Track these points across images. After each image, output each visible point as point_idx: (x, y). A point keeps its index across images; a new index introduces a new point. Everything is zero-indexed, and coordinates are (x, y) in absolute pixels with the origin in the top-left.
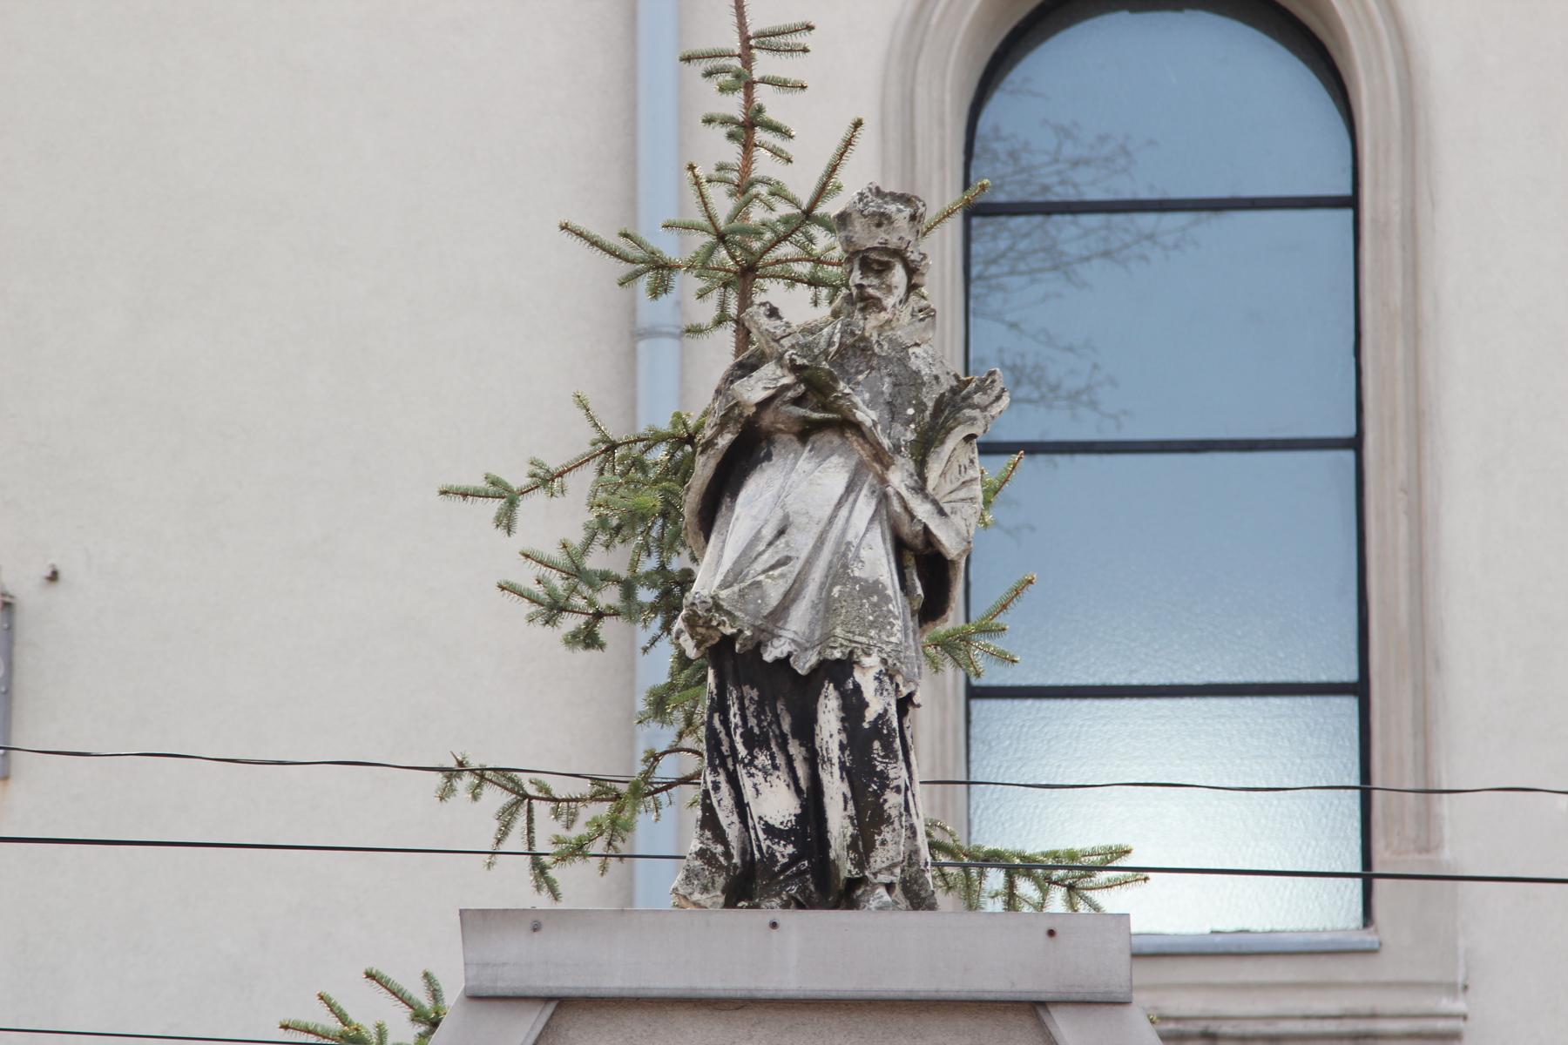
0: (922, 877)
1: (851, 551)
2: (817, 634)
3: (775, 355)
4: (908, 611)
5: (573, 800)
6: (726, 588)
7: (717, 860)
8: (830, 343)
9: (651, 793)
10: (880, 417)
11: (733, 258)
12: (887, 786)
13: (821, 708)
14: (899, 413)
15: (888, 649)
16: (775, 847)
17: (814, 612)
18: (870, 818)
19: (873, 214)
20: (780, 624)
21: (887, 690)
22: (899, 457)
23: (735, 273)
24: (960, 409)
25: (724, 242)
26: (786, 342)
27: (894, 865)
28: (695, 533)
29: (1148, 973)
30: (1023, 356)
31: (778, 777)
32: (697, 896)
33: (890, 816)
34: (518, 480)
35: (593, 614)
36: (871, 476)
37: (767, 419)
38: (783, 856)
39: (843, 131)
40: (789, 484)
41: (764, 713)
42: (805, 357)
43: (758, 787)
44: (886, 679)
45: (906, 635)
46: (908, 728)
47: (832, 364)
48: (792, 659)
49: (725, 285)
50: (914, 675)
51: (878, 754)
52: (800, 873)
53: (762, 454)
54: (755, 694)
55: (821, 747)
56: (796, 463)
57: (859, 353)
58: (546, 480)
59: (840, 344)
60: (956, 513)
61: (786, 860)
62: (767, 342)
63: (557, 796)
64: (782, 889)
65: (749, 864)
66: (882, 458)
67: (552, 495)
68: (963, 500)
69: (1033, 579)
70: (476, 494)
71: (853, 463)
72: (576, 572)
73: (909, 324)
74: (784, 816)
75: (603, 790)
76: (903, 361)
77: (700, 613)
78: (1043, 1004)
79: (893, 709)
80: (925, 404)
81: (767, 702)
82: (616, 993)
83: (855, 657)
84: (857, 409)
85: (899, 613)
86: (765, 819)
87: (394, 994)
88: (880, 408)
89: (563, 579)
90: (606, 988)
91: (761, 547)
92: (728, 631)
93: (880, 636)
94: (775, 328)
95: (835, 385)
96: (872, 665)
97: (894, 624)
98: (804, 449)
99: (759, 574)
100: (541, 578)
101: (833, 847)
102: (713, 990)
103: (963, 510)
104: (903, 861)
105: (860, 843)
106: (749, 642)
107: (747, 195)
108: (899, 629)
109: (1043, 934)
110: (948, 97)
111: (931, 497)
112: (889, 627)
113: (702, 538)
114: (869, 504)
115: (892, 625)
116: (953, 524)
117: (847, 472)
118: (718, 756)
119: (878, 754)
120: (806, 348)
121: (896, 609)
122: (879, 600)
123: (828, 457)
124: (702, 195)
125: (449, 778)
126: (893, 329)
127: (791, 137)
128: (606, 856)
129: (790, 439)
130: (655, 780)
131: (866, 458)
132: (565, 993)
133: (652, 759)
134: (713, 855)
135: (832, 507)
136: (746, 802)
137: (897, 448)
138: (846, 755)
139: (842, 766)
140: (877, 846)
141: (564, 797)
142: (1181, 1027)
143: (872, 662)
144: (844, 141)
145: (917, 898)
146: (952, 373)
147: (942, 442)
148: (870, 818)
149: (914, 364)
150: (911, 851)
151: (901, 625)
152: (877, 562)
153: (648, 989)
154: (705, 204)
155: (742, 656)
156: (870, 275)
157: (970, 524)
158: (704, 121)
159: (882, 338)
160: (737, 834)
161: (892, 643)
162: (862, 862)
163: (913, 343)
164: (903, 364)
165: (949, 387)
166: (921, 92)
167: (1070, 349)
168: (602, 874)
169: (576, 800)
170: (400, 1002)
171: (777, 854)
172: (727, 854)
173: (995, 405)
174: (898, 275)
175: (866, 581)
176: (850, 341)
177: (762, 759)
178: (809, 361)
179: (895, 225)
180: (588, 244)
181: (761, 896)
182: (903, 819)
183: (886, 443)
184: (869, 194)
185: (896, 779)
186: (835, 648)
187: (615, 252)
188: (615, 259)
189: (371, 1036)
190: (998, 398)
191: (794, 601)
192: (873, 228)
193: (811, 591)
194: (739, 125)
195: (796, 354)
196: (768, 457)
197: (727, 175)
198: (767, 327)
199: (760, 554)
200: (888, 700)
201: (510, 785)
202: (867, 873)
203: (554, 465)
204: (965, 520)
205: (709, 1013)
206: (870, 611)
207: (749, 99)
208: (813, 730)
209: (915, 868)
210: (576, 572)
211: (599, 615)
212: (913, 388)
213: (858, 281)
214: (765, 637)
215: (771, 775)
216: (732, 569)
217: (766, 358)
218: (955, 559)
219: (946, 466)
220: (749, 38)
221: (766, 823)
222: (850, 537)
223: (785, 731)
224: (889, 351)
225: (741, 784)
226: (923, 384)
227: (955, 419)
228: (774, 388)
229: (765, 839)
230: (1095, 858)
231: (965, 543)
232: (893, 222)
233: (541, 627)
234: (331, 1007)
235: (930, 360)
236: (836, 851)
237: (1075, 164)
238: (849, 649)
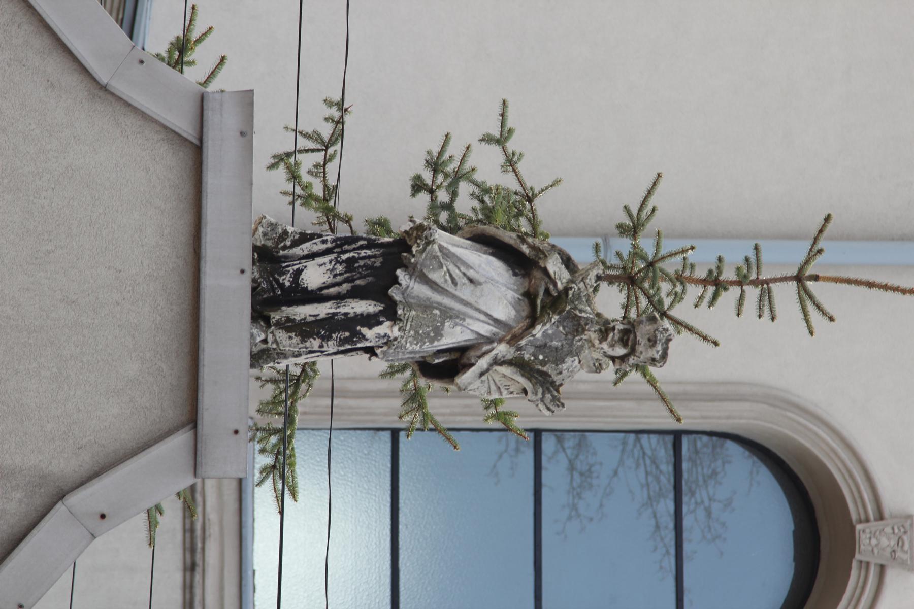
0: (271, 361)
1: (460, 321)
2: (412, 301)
3: (574, 279)
4: (425, 354)
5: (324, 175)
6: (439, 249)
7: (282, 242)
8: (581, 311)
9: (328, 220)
10: (538, 339)
11: (639, 271)
12: (323, 340)
13: (369, 302)
14: (540, 350)
15: (403, 341)
16: (289, 275)
17: (425, 299)
18: (305, 330)
19: (655, 336)
20: (418, 279)
21: (379, 340)
22: (514, 350)
23: (631, 273)
24: (542, 386)
25: (648, 266)
26: (582, 285)
27: (277, 344)
28: (472, 232)
30: (598, 477)
31: (329, 277)
32: (261, 230)
33: (306, 341)
34: (511, 146)
35: (432, 188)
36: (504, 333)
37: (537, 274)
38: (283, 280)
39: (712, 335)
40: (500, 286)
41: (367, 270)
42: (573, 296)
43: (324, 266)
44: (385, 340)
45: (411, 353)
46: (357, 353)
47: (569, 311)
48: (397, 286)
49: (624, 268)
50: (388, 357)
51: (342, 335)
52: (273, 290)
53: (517, 271)
54: (378, 264)
55: (346, 302)
56: (511, 290)
57: (575, 328)
58: (511, 162)
59: (581, 317)
60: (482, 383)
61: (281, 281)
62: (582, 274)
63: (327, 166)
64: (264, 279)
65: (278, 260)
66: (513, 340)
67: (502, 166)
68: (489, 387)
69: (457, 449)
71: (511, 323)
72: (458, 176)
73: (592, 357)
74: (306, 280)
75: (331, 192)
76: (570, 353)
77: (425, 233)
78: (195, 427)
79: (368, 344)
80: (545, 366)
81: (372, 271)
82: (204, 179)
83: (398, 322)
84: (543, 326)
85: (424, 349)
86: (305, 269)
87: (212, 72)
88: (543, 339)
89: (454, 169)
90: (207, 174)
91: (462, 269)
92: (414, 249)
93: (410, 337)
94: (590, 279)
95: (556, 313)
96: (394, 332)
97: (417, 345)
98: (519, 295)
99: (447, 267)
100: (453, 158)
101: (288, 309)
102: (206, 236)
103: (483, 387)
104: (280, 349)
105: (290, 324)
106: (407, 261)
107: (676, 280)
108: (414, 348)
109: (236, 427)
110: (743, 421)
111: (490, 368)
112: (415, 342)
113: (469, 236)
114: (487, 332)
115: (417, 344)
116: (476, 381)
117: (506, 319)
118: (341, 244)
119: (342, 335)
120: (578, 297)
121: (426, 347)
122: (431, 337)
123: (515, 309)
124: (676, 254)
125: (337, 104)
126: (589, 348)
127: (709, 307)
128: (294, 195)
129: (525, 287)
130: (336, 222)
131: (514, 330)
132: (205, 150)
133: (347, 219)
134: (285, 240)
135: (485, 310)
136: (315, 259)
137: (519, 349)
138: (341, 316)
139: (335, 314)
140: (289, 334)
141: (326, 170)
142: (199, 550)
143: (395, 332)
144: (706, 336)
145: (259, 357)
146: (563, 382)
147: (523, 375)
148: (305, 330)
149: (569, 360)
150: (286, 355)
151: (417, 349)
152: (453, 336)
153: (207, 199)
154: (671, 255)
155: (400, 258)
156: (621, 334)
157: (475, 391)
158: (720, 257)
159: (584, 341)
160: (297, 253)
161: (406, 344)
162: (279, 325)
163: (581, 359)
164: (569, 354)
165: (555, 380)
166: (747, 405)
167: (601, 506)
168: (281, 193)
169: (325, 177)
170: (208, 76)
171: (284, 277)
172: (285, 248)
173: (544, 407)
174: (620, 351)
175: (442, 329)
176: (582, 322)
177: (340, 268)
178: (571, 298)
179: (649, 349)
180: (649, 188)
181: (261, 267)
182: (304, 350)
183: (523, 342)
184: (667, 335)
185: (328, 345)
186: (403, 310)
187: (644, 204)
188: (640, 204)
189: (188, 57)
190: (549, 409)
191: (431, 287)
192: (647, 337)
193: (437, 298)
194: (717, 278)
195: (575, 291)
196: (515, 274)
197: (688, 269)
198: (590, 275)
199: (459, 269)
200: (373, 341)
201: (333, 138)
202: (273, 328)
203: (520, 166)
204: (478, 388)
205: (192, 234)
206: (425, 332)
207: (733, 283)
208: (356, 298)
209: (276, 357)
210: (458, 176)
211: (431, 192)
212: (554, 359)
213: (617, 327)
214: (411, 271)
215: (331, 273)
216: (450, 252)
217: (573, 274)
218: (455, 382)
219: (509, 377)
220: (768, 284)
221: (302, 270)
222: (468, 320)
223: (356, 282)
224: (576, 346)
225: (326, 256)
226: (557, 365)
227: (536, 383)
228: (555, 277)
229: (293, 269)
230: (291, 479)
231: (464, 388)
232: (651, 348)
233: (424, 158)
234: (205, 34)
235: (571, 369)
236: (286, 310)
237: (709, 513)
238: (403, 319)
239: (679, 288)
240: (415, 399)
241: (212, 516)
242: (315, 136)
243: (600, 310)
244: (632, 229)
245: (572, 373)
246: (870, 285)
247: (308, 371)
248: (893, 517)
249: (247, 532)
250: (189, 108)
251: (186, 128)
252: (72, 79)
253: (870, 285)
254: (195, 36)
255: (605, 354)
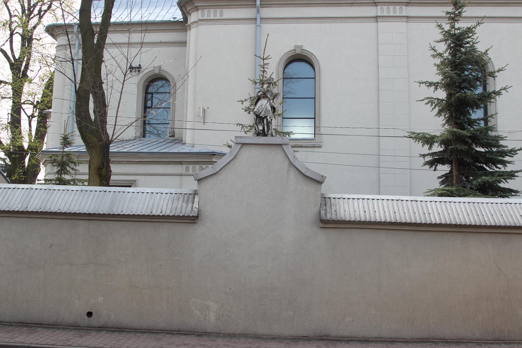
18: (268, 129)
29: (290, 141)
39: (272, 73)
58: (246, 100)
65: (259, 133)
66: (270, 100)
70: (240, 101)
75: (250, 126)
76: (272, 92)
78: (282, 144)
118: (256, 124)
120: (264, 91)
143: (269, 116)
145: (272, 136)
148: (268, 129)
149: (273, 92)
152: (269, 108)
162: (268, 133)
167: (293, 89)
174: (272, 85)
177: (260, 124)
183: (270, 98)
193: (264, 111)
207: (264, 69)
237: (294, 74)
239: (264, 77)
240: (279, 115)
241: (294, 144)
242: (242, 128)
243: (266, 88)
244: (256, 83)
245: (275, 92)
246: (265, 49)
247: (275, 130)
248: (295, 48)
249: (297, 139)
250: (237, 145)
251: (240, 146)
252: (233, 161)
253: (265, 49)
254: (228, 144)
255: (272, 87)
